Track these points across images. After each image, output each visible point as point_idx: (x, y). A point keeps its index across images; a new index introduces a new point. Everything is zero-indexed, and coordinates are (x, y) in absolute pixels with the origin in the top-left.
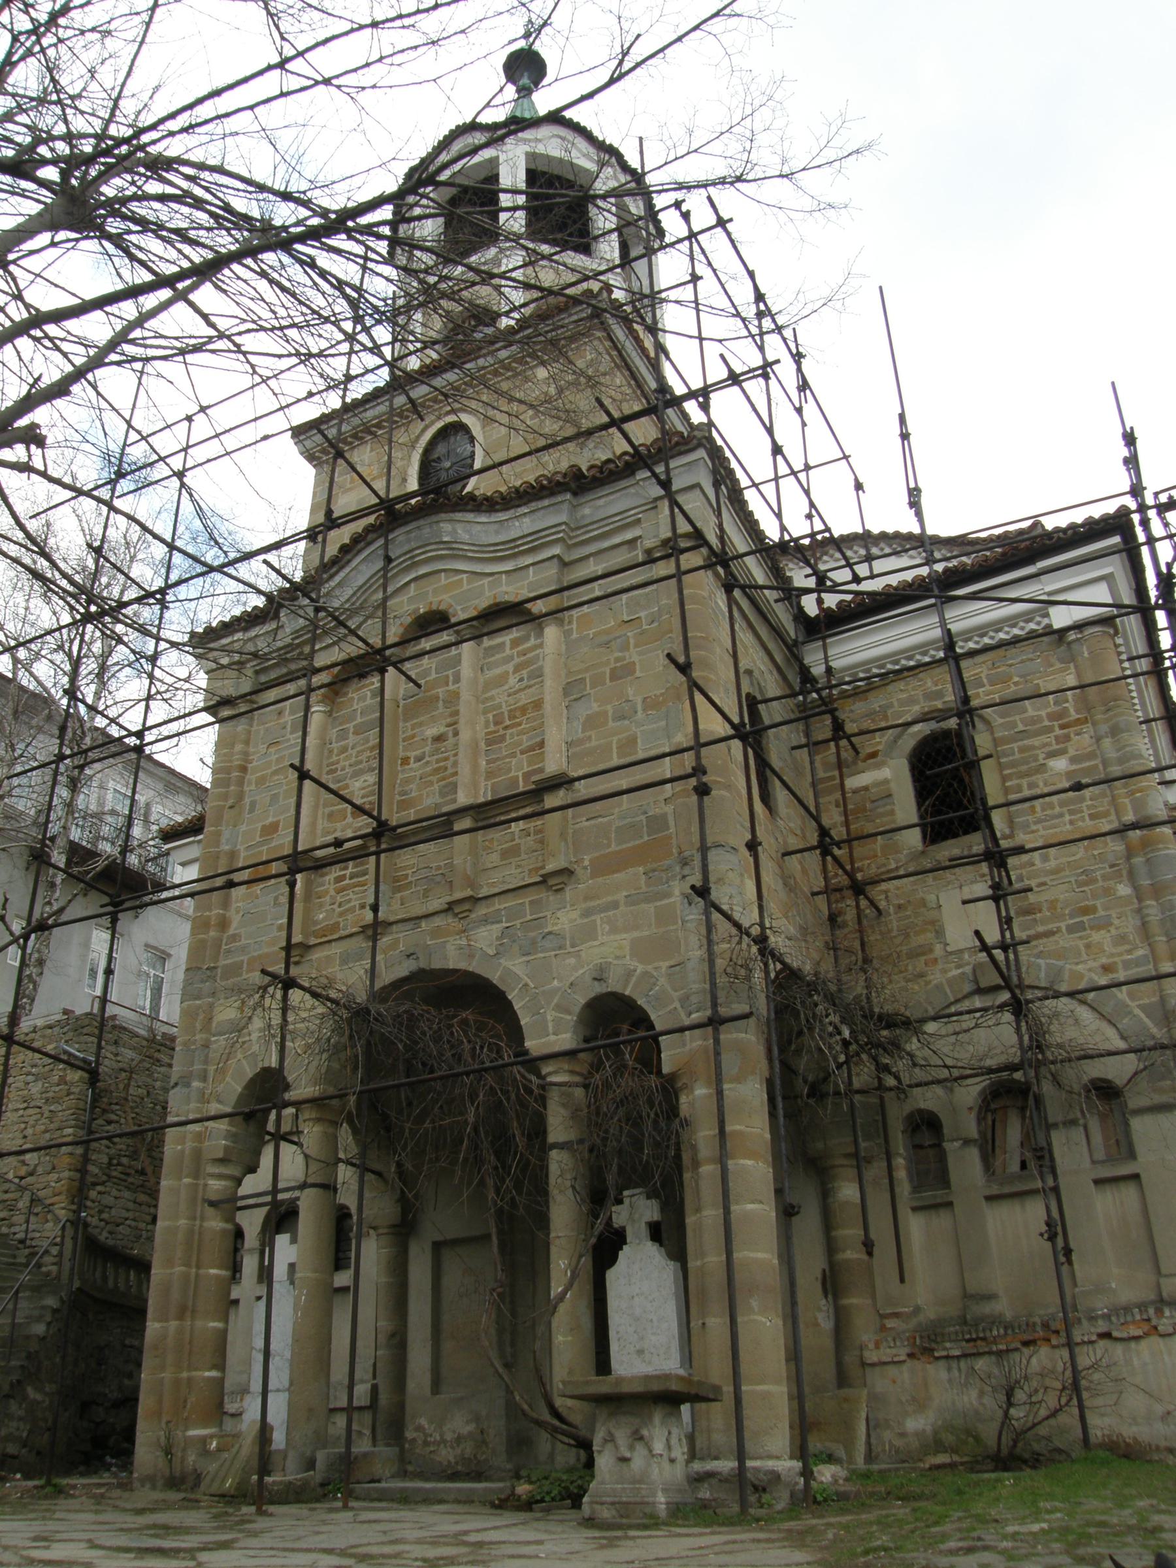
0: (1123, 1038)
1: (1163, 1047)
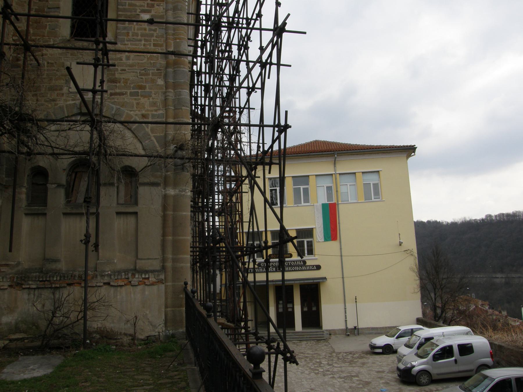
0: (144, 149)
1: (161, 157)
